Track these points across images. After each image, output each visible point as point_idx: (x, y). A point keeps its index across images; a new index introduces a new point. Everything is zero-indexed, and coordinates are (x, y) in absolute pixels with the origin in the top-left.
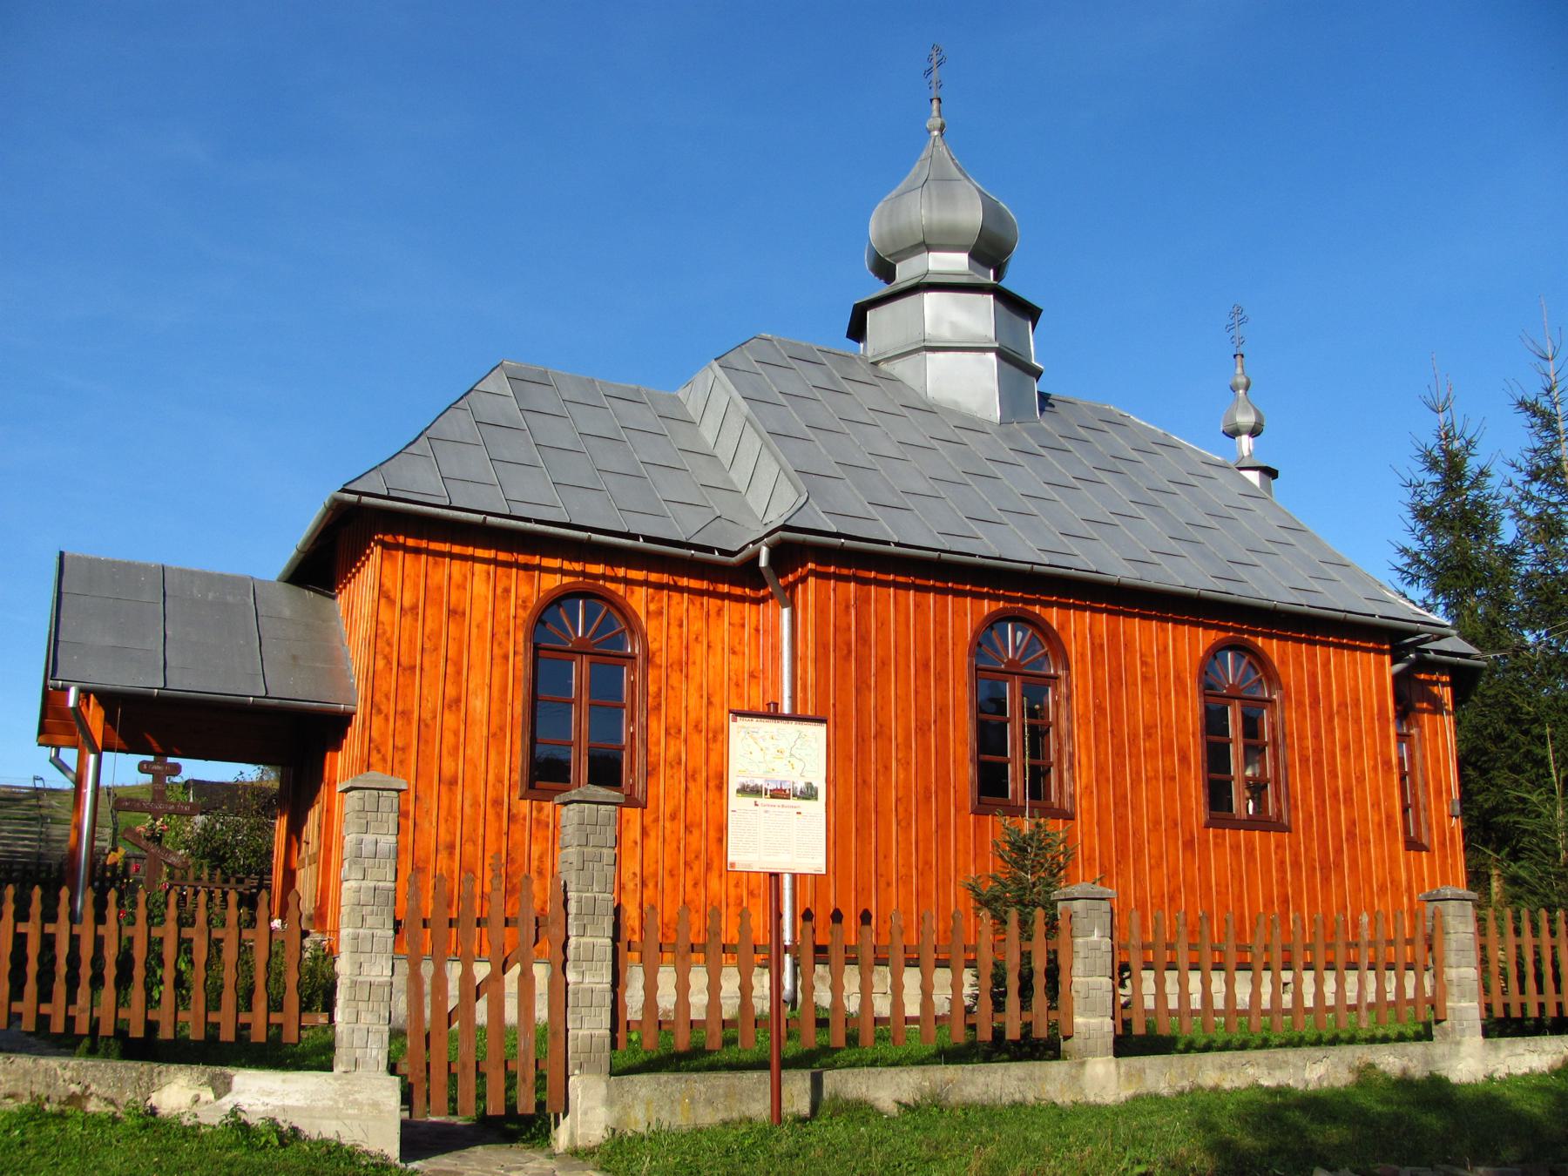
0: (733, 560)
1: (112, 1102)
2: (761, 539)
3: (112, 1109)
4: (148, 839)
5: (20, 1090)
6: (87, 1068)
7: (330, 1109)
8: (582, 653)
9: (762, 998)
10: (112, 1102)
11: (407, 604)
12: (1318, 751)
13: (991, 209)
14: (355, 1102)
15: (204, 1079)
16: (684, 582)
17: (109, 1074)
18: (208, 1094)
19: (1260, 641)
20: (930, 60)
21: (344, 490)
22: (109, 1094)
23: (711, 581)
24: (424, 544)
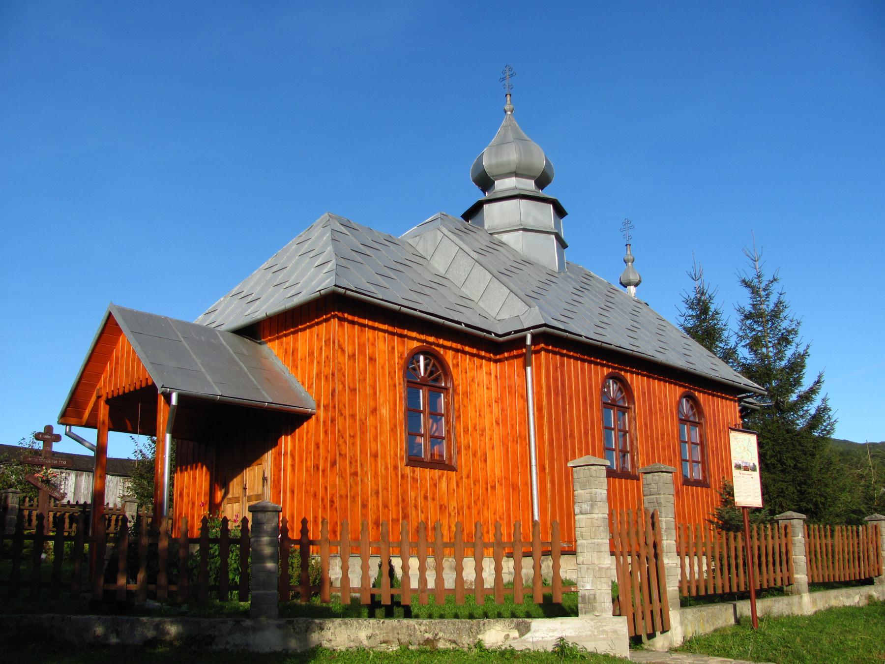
0: (501, 339)
1: (455, 642)
2: (529, 329)
3: (454, 645)
4: (43, 481)
5: (391, 639)
6: (436, 624)
7: (590, 636)
8: (425, 385)
9: (510, 573)
10: (455, 642)
11: (350, 353)
12: (717, 448)
13: (547, 162)
14: (604, 632)
15: (513, 625)
16: (467, 349)
17: (451, 626)
18: (515, 634)
19: (696, 393)
20: (504, 72)
21: (335, 285)
22: (452, 637)
23: (478, 349)
24: (356, 319)
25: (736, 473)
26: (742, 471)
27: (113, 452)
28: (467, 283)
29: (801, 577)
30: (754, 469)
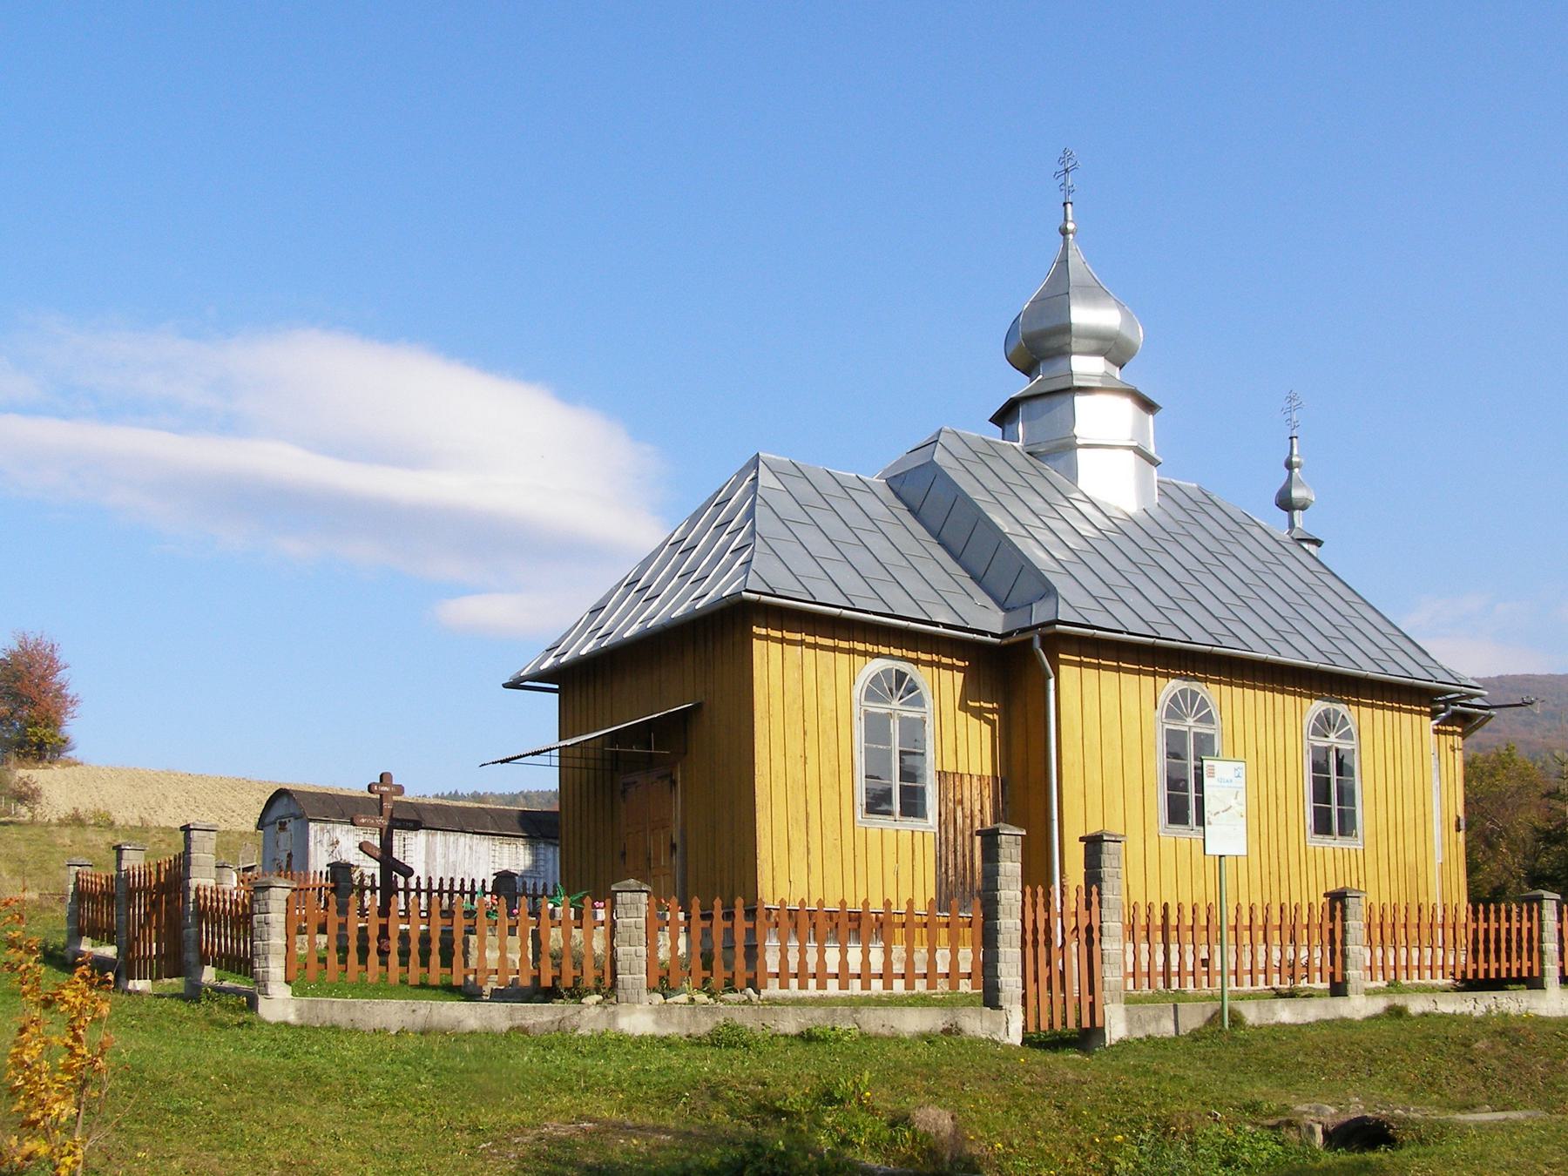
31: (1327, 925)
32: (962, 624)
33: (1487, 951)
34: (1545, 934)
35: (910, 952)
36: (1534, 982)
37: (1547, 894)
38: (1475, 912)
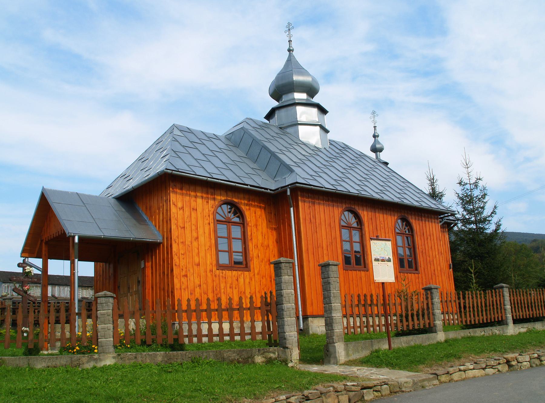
25: (375, 263)
26: (380, 262)
27: (51, 271)
28: (258, 160)
29: (439, 323)
30: (389, 260)
31: (457, 301)
32: (258, 185)
33: (532, 307)
34: (506, 302)
35: (242, 322)
36: (501, 322)
37: (504, 285)
38: (458, 294)
